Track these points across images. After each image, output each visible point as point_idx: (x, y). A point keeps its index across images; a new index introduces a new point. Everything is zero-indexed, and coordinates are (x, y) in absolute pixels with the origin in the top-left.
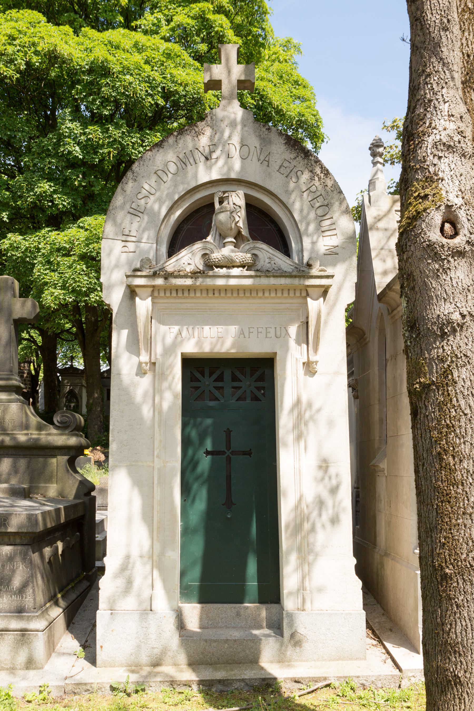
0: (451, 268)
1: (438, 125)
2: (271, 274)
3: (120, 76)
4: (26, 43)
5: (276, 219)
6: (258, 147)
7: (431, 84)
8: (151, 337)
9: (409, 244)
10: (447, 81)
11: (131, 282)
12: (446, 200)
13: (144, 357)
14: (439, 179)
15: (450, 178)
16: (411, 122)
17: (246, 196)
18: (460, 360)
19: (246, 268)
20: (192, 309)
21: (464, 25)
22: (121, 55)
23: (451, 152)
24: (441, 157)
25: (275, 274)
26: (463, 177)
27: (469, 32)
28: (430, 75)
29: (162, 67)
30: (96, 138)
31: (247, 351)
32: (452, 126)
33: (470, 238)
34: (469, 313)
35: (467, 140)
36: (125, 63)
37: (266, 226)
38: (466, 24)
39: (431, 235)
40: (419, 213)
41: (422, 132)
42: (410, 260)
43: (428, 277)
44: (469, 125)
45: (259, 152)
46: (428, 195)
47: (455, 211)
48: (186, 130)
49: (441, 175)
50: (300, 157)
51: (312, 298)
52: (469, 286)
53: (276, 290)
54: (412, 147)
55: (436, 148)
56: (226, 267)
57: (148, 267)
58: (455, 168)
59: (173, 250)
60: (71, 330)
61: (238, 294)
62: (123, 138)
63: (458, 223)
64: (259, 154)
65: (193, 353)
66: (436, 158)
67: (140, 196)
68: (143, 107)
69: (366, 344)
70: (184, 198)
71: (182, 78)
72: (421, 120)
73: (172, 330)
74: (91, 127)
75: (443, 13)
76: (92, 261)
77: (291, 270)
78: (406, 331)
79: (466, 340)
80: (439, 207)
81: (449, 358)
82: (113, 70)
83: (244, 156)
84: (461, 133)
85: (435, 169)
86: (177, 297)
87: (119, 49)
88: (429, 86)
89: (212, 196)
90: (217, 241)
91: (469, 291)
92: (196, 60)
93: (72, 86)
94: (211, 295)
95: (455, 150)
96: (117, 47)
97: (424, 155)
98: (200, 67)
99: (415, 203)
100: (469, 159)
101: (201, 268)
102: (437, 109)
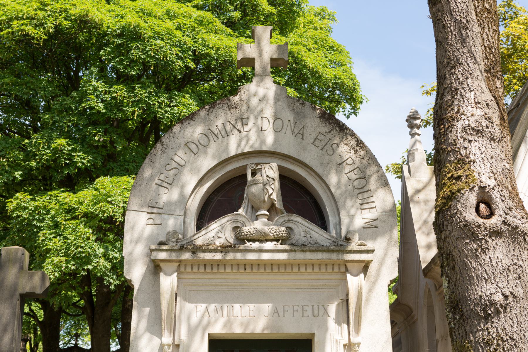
0: (489, 248)
1: (466, 111)
2: (307, 249)
3: (151, 40)
4: (57, 9)
5: (311, 191)
6: (292, 121)
7: (456, 74)
8: (175, 316)
9: (446, 223)
10: (471, 72)
11: (155, 256)
12: (478, 181)
13: (167, 339)
14: (471, 161)
15: (481, 161)
16: (440, 107)
17: (280, 168)
18: (506, 343)
19: (280, 241)
20: (222, 285)
21: (484, 23)
22: (152, 20)
23: (480, 136)
24: (471, 141)
25: (311, 248)
26: (493, 160)
27: (489, 29)
28: (455, 67)
29: (193, 33)
30: (121, 96)
31: (282, 332)
32: (479, 113)
33: (506, 218)
34: (512, 293)
35: (494, 126)
36: (157, 29)
37: (301, 198)
38: (486, 22)
39: (466, 215)
40: (453, 193)
41: (451, 117)
42: (448, 239)
43: (467, 257)
44: (495, 111)
45: (293, 125)
46: (461, 176)
47: (488, 192)
48: (219, 104)
49: (472, 157)
50: (335, 130)
51: (351, 274)
52: (509, 266)
53: (313, 265)
54: (443, 130)
55: (466, 132)
56: (258, 240)
57: (174, 240)
58: (486, 151)
59: (202, 223)
60: (78, 304)
61: (272, 269)
62: (149, 98)
63: (493, 204)
64: (293, 128)
65: (221, 334)
66: (466, 141)
67: (168, 167)
68: (172, 70)
69: (414, 322)
70: (215, 170)
71: (214, 43)
72: (449, 106)
73: (199, 308)
74: (115, 86)
75: (462, 15)
76: (110, 229)
77: (328, 244)
78: (449, 312)
79: (511, 322)
80: (473, 188)
81: (495, 342)
82: (144, 35)
83: (277, 129)
84: (488, 119)
85: (466, 152)
86: (205, 272)
87: (150, 16)
88: (455, 77)
89: (245, 167)
90: (249, 214)
91: (510, 271)
92: (228, 27)
93: (100, 48)
94: (242, 270)
95: (484, 134)
96: (150, 15)
97: (454, 138)
98: (232, 33)
99: (449, 184)
100: (498, 142)
101: (232, 241)
102: (464, 97)
